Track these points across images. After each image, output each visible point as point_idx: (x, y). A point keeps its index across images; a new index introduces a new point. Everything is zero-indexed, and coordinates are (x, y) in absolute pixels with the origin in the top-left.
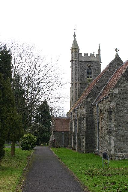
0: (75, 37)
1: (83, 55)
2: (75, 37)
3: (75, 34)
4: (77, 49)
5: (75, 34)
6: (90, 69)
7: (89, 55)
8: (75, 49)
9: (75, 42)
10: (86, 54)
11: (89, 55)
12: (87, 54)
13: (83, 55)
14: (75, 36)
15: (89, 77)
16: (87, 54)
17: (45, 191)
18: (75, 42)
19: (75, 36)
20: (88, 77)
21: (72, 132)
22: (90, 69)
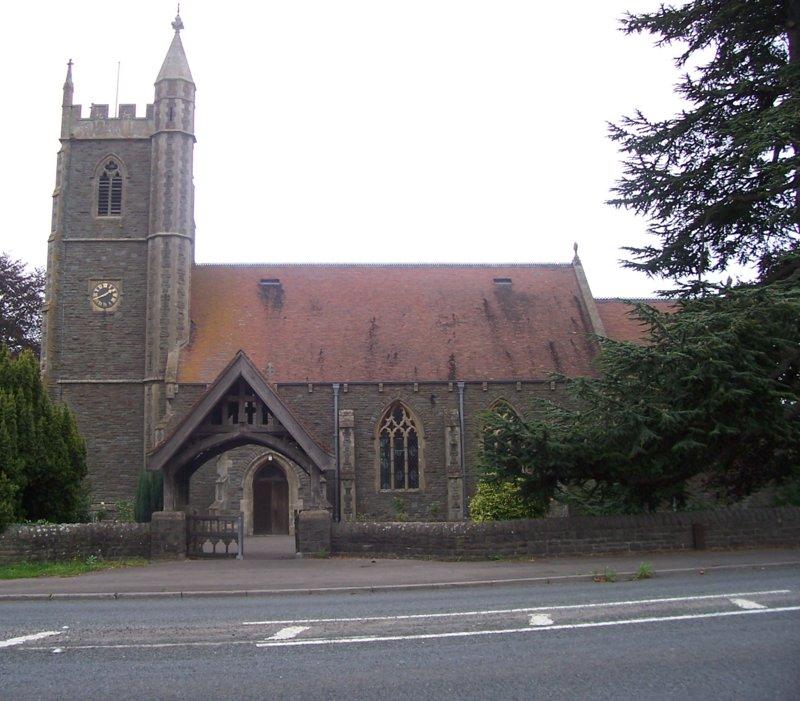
0: (177, 33)
1: (86, 114)
2: (177, 33)
3: (178, 19)
4: (181, 85)
5: (178, 19)
6: (117, 175)
7: (113, 113)
8: (172, 82)
9: (176, 47)
10: (100, 110)
11: (113, 113)
12: (104, 109)
13: (86, 114)
14: (178, 25)
15: (110, 207)
16: (104, 109)
17: (247, 699)
18: (176, 47)
19: (178, 25)
20: (103, 211)
21: (641, 177)
22: (117, 175)
